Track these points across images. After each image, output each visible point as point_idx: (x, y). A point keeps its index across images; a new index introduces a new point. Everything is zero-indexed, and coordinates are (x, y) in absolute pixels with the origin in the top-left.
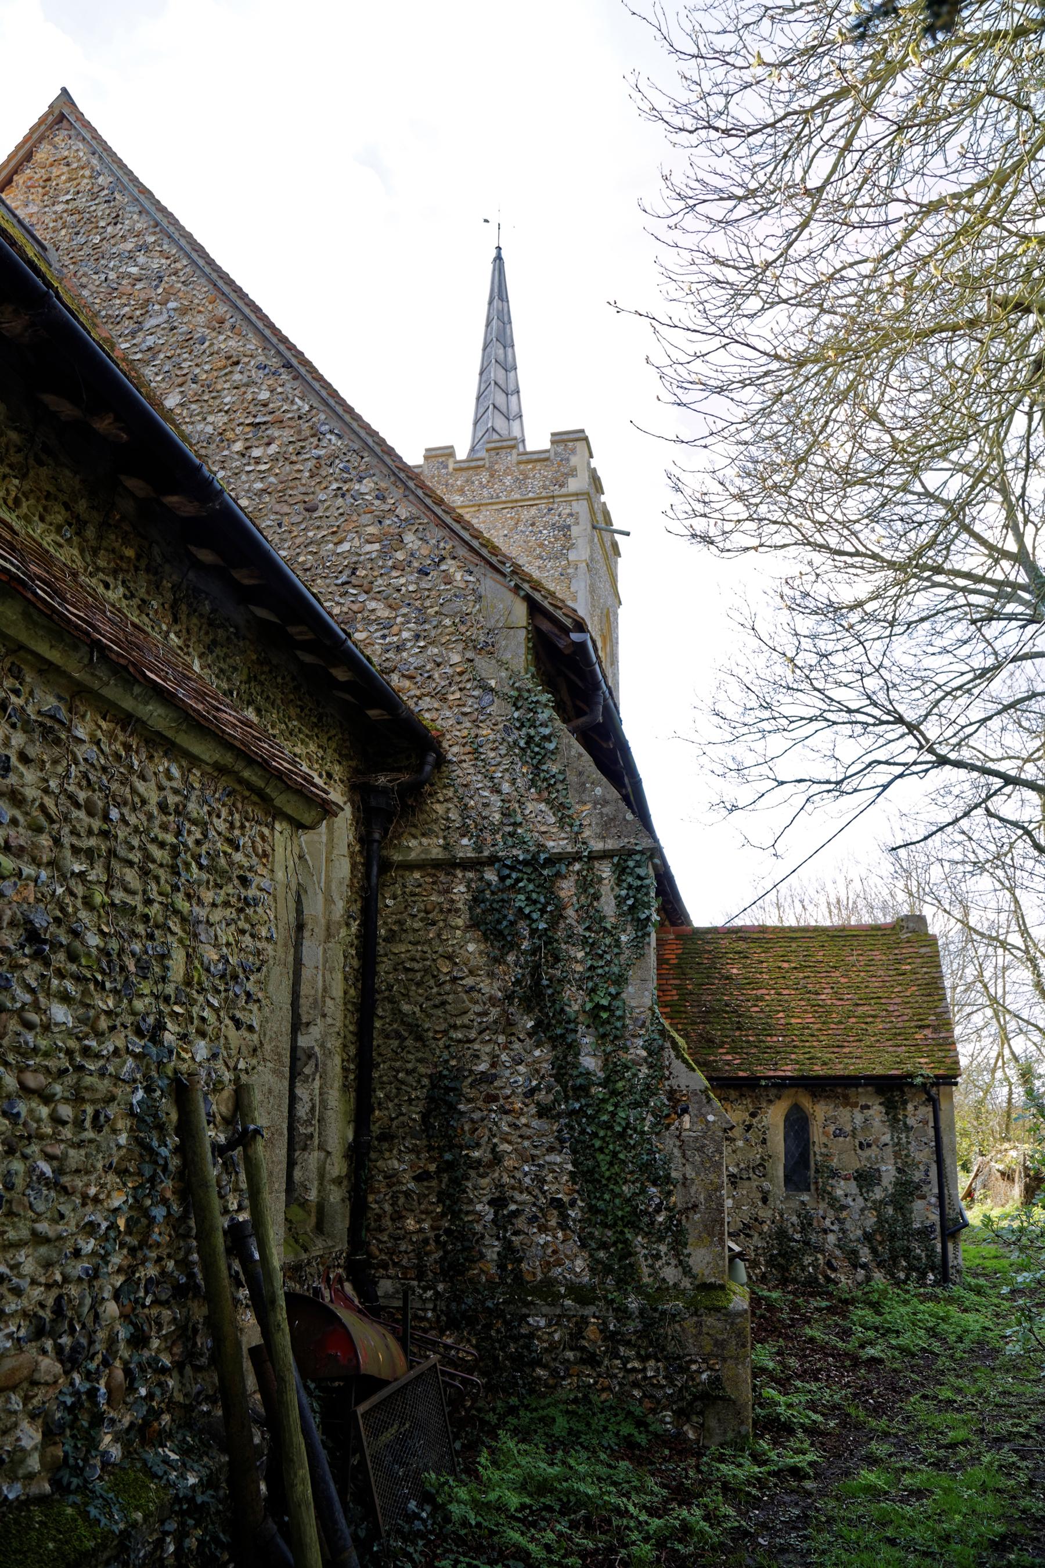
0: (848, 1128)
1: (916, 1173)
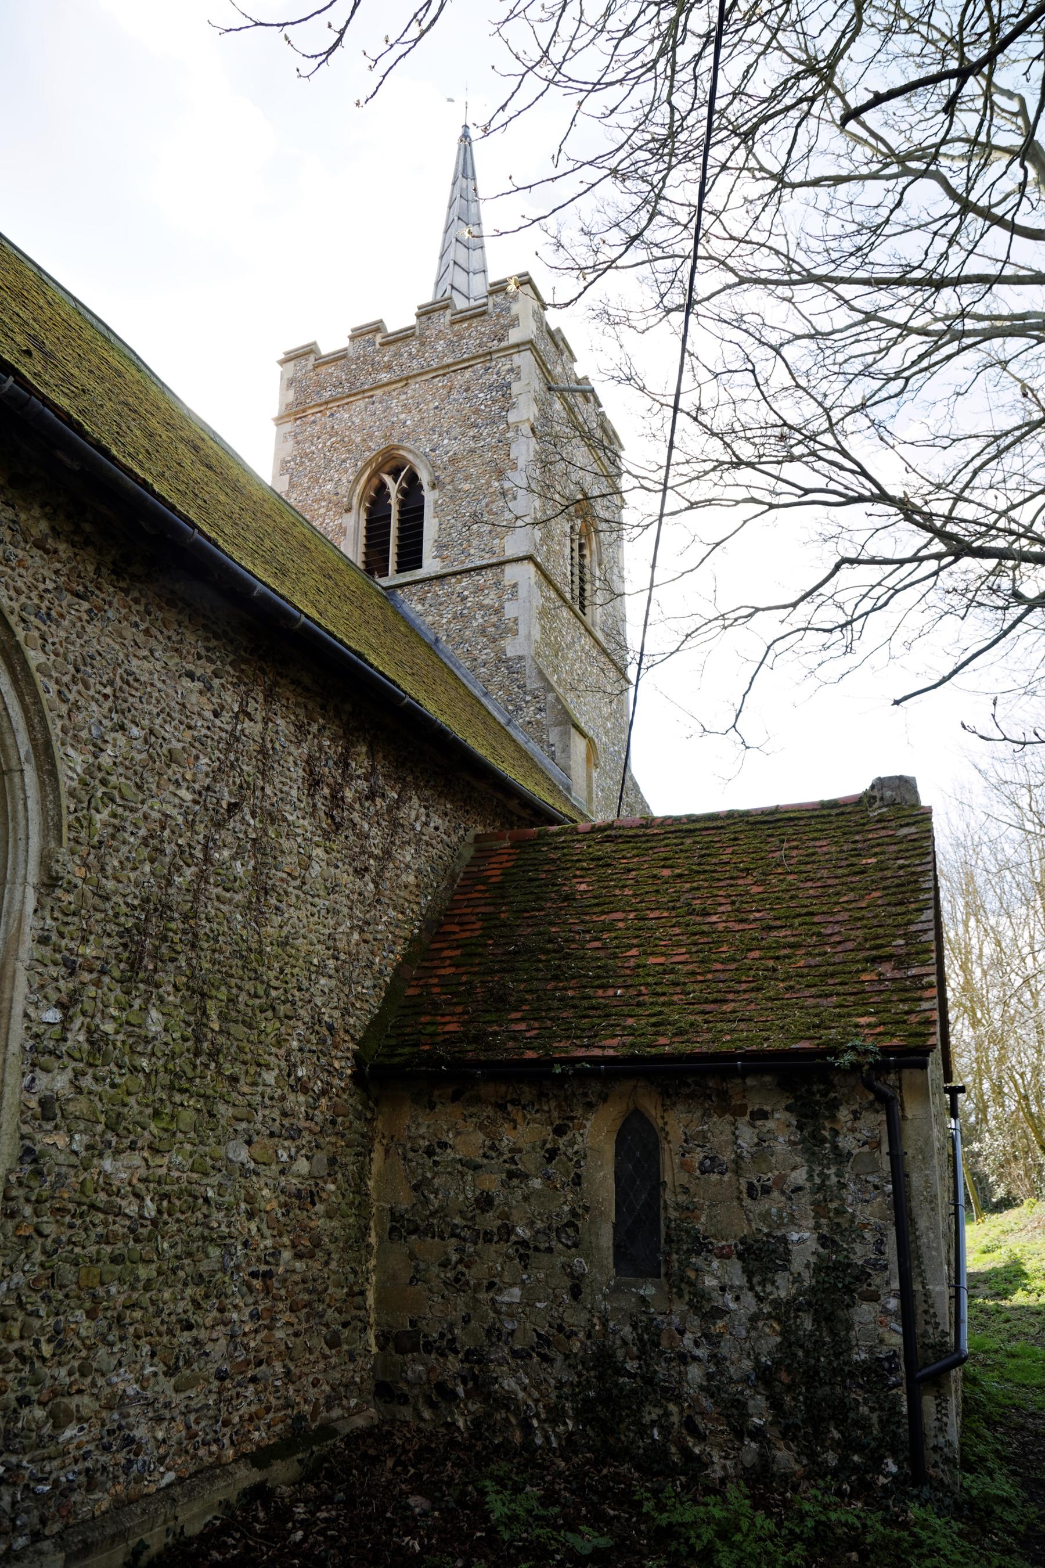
0: (727, 1156)
1: (858, 1248)
